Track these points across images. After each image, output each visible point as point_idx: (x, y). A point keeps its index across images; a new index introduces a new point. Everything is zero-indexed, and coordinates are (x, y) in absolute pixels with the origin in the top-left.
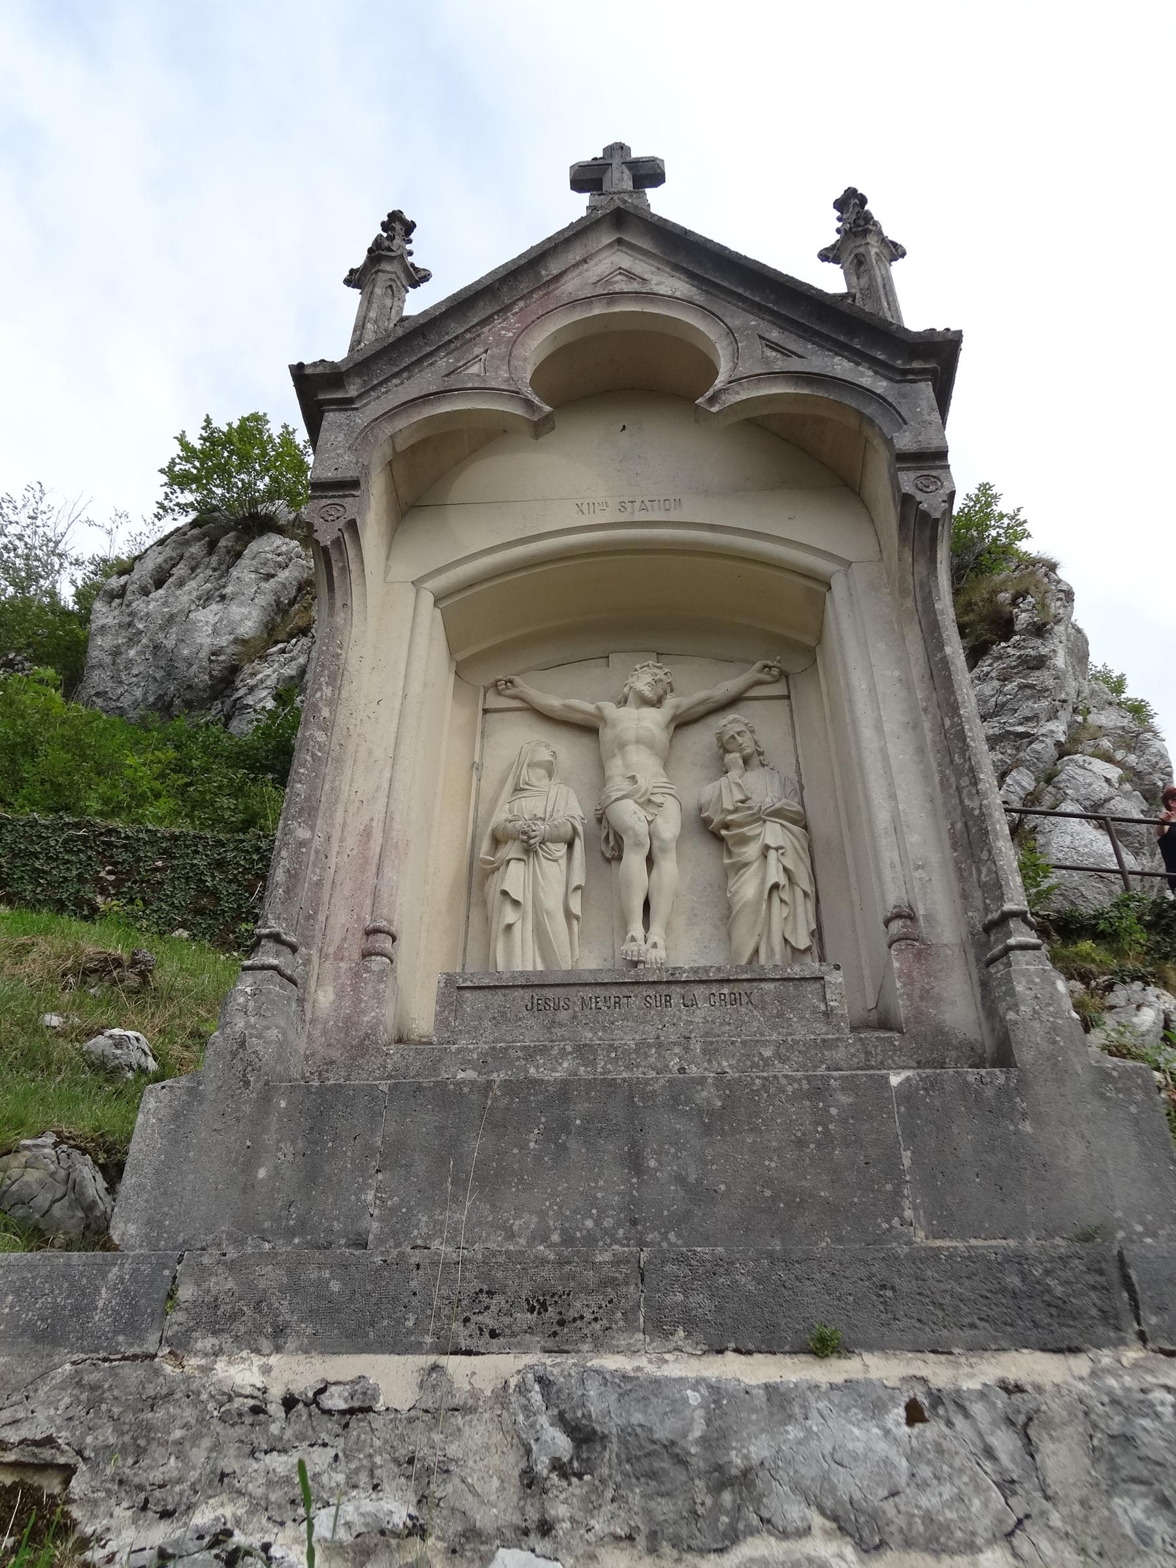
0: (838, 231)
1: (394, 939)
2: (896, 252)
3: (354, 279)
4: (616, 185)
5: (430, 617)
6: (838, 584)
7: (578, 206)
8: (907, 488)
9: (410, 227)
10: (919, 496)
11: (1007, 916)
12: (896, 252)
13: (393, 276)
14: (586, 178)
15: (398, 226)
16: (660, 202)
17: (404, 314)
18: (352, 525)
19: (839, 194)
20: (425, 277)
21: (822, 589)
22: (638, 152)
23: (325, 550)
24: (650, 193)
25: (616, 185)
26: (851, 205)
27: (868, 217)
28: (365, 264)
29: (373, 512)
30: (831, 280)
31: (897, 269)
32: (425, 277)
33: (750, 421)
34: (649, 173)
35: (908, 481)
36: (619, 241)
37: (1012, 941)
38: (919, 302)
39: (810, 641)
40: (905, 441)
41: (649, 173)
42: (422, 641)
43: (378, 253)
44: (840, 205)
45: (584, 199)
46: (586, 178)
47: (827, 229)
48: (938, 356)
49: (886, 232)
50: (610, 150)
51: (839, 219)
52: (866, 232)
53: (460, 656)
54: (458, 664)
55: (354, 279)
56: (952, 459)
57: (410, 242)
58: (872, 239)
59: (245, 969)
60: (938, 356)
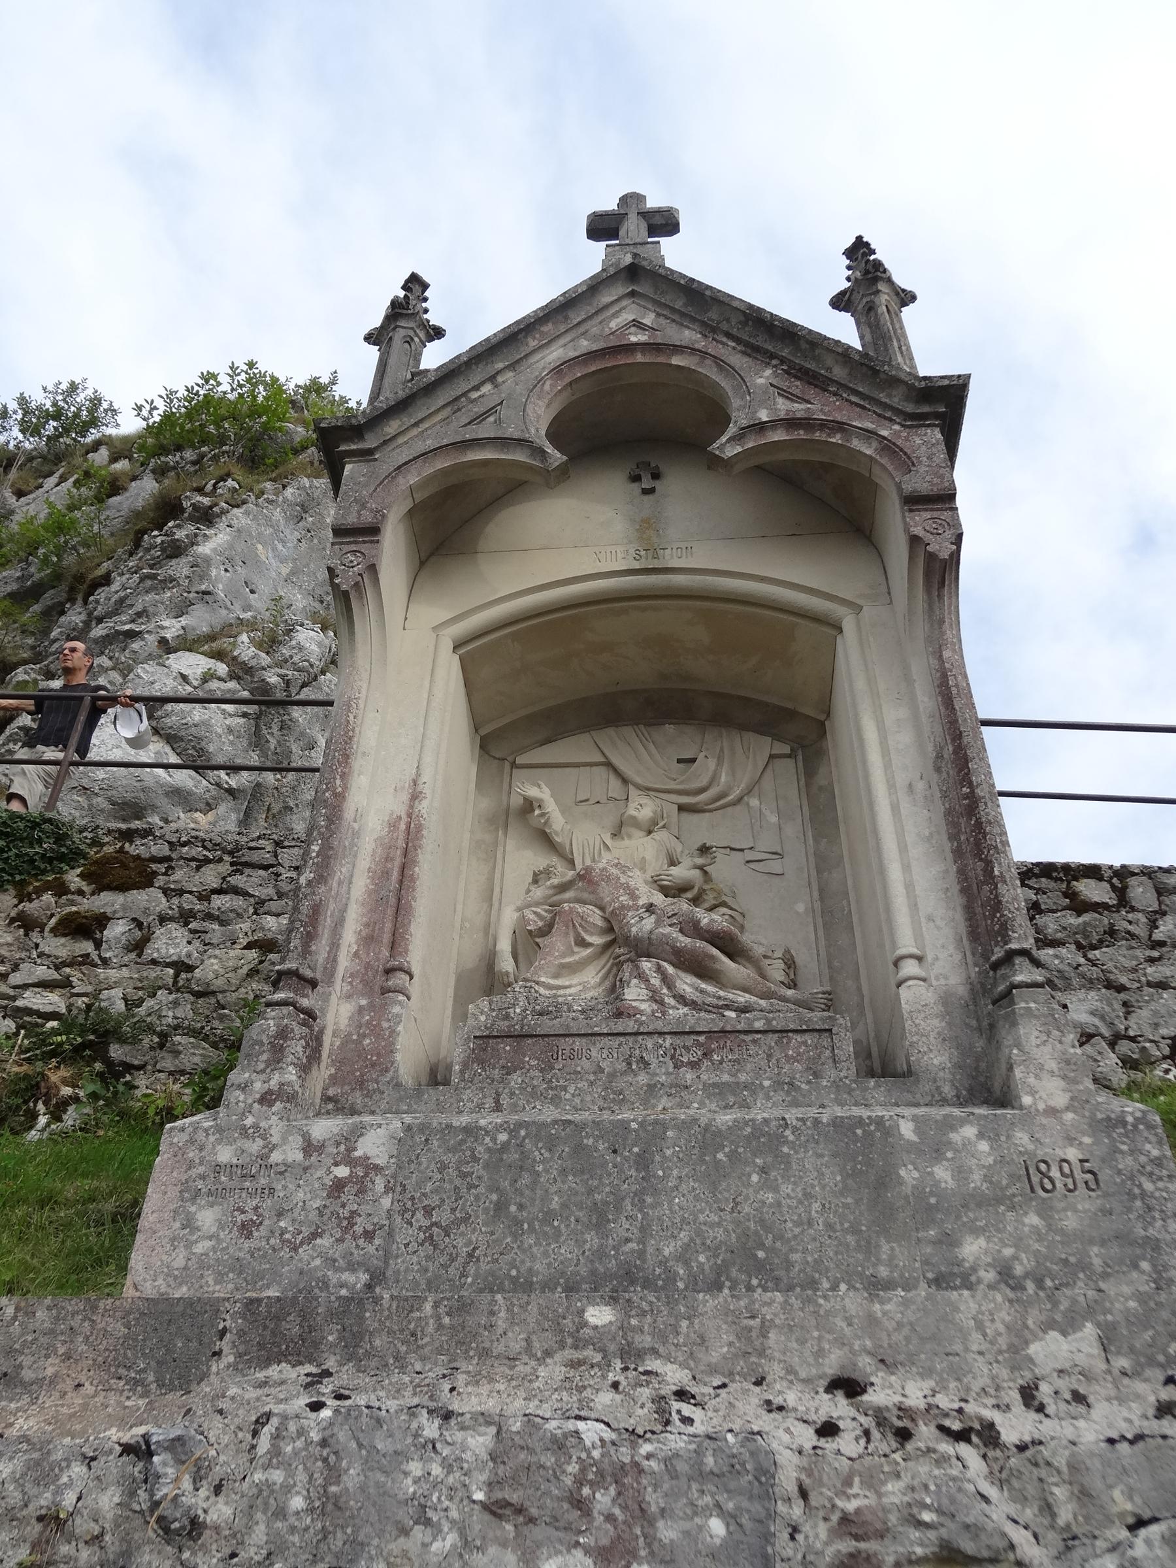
0: (848, 279)
1: (411, 978)
2: (907, 298)
3: (372, 338)
4: (630, 228)
5: (450, 670)
6: (848, 624)
7: (592, 258)
8: (918, 531)
9: (425, 286)
10: (927, 537)
11: (1011, 955)
12: (907, 298)
13: (411, 333)
14: (602, 227)
15: (415, 284)
16: (677, 254)
17: (422, 367)
18: (373, 569)
19: (849, 241)
20: (437, 333)
21: (834, 632)
22: (653, 202)
23: (346, 594)
24: (664, 241)
25: (630, 228)
26: (859, 251)
27: (878, 265)
28: (382, 327)
29: (393, 552)
30: (844, 330)
31: (908, 314)
32: (437, 333)
33: (759, 468)
34: (665, 223)
35: (920, 522)
36: (633, 294)
37: (1019, 978)
38: (931, 345)
39: (822, 717)
40: (918, 482)
41: (665, 223)
42: (441, 673)
43: (399, 311)
44: (850, 253)
45: (599, 249)
46: (602, 227)
47: (838, 278)
48: (944, 403)
49: (895, 279)
50: (624, 200)
51: (849, 268)
52: (876, 280)
53: (483, 732)
54: (482, 738)
55: (372, 338)
56: (960, 501)
57: (425, 300)
58: (881, 286)
59: (268, 1005)
60: (944, 403)
